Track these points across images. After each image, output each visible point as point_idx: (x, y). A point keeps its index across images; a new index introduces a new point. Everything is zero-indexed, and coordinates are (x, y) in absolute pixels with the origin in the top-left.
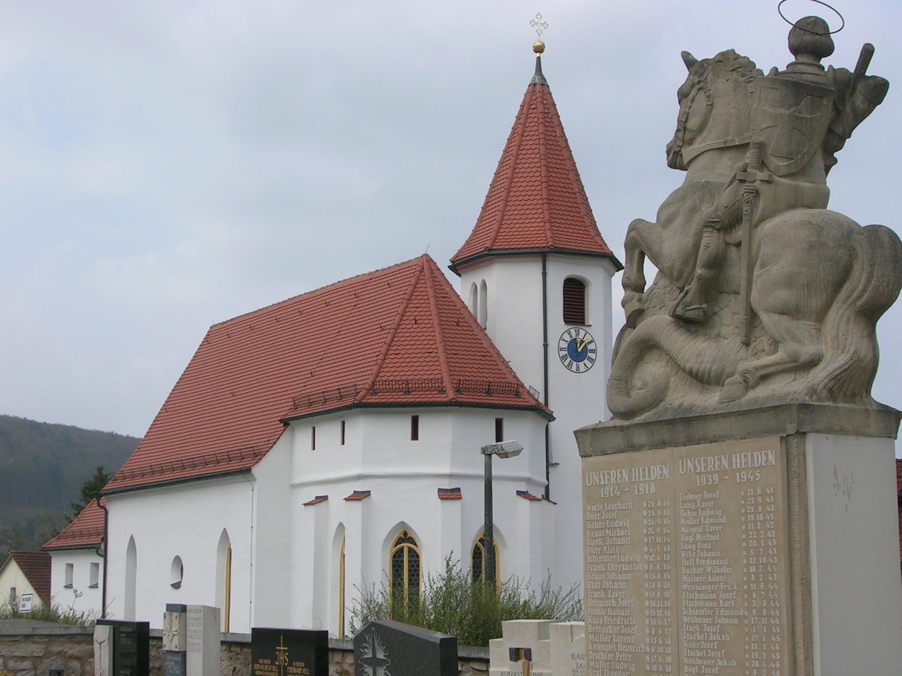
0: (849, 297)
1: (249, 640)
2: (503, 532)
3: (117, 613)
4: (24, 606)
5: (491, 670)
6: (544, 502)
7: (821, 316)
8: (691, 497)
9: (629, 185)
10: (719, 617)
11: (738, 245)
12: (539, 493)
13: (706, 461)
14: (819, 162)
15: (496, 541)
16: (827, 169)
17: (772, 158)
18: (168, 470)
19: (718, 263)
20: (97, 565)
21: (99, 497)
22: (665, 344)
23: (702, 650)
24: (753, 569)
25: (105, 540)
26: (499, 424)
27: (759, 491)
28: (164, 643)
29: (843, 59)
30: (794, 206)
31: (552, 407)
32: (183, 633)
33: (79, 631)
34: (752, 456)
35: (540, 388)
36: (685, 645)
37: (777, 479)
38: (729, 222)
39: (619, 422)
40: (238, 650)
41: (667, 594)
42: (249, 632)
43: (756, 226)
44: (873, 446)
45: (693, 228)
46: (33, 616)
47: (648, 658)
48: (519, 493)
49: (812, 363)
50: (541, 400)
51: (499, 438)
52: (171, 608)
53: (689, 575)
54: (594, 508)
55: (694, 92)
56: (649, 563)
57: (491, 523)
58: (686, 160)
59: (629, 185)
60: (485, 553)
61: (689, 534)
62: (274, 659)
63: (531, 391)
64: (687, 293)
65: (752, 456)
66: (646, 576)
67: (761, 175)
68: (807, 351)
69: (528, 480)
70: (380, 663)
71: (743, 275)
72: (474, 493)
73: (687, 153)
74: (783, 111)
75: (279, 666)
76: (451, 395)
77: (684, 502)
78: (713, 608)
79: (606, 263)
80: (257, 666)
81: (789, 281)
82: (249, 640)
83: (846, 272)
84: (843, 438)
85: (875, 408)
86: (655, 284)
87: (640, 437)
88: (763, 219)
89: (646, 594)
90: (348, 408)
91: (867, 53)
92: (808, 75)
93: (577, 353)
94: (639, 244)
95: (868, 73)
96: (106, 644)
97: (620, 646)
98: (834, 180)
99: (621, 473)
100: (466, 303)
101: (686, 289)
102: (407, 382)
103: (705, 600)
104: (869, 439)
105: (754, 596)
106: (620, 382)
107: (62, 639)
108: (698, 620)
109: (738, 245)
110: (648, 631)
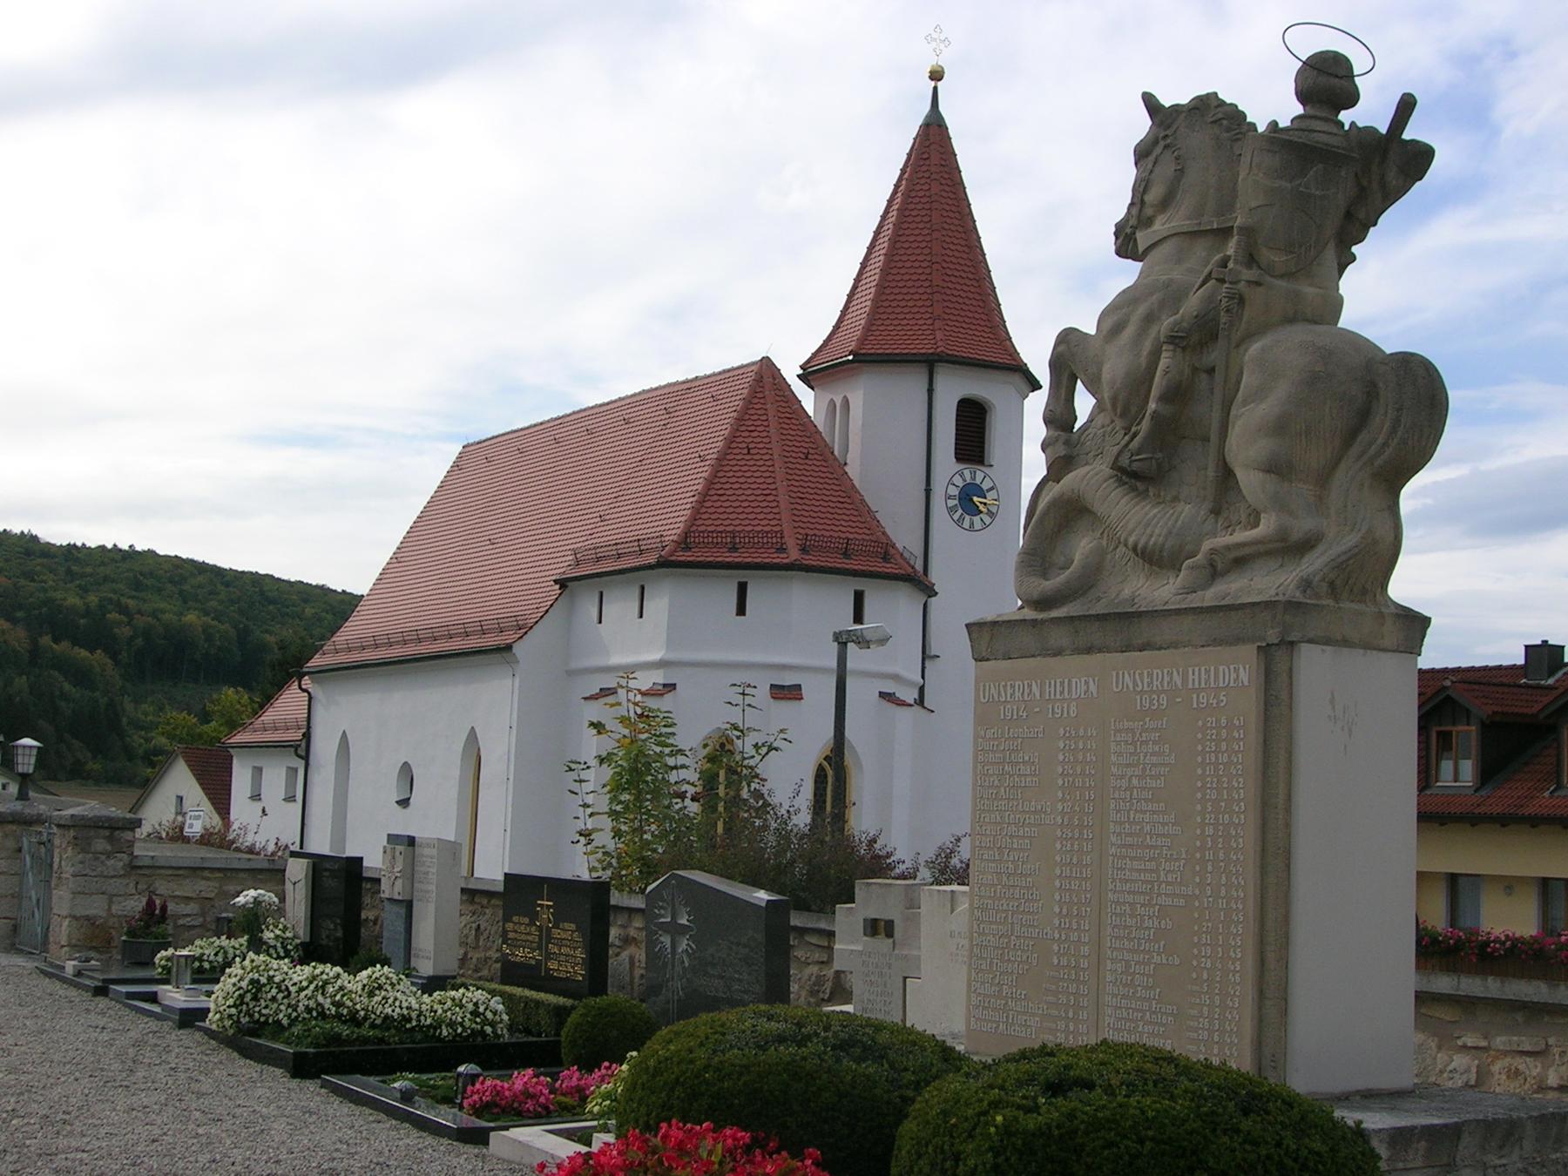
0: (1363, 453)
1: (501, 888)
2: (859, 750)
3: (320, 843)
4: (191, 826)
5: (837, 946)
6: (917, 708)
7: (1323, 479)
8: (1127, 724)
9: (1055, 268)
10: (1159, 895)
11: (1211, 371)
12: (910, 695)
13: (1150, 675)
14: (1330, 255)
15: (848, 759)
16: (1341, 270)
17: (1264, 251)
18: (398, 643)
19: (1177, 394)
20: (296, 770)
21: (301, 676)
22: (1100, 508)
23: (1133, 940)
24: (1209, 831)
25: (307, 736)
26: (859, 598)
27: (1223, 721)
28: (383, 887)
29: (1370, 111)
30: (1291, 320)
31: (936, 576)
32: (410, 874)
33: (266, 865)
34: (1216, 670)
35: (918, 550)
36: (1109, 930)
37: (1249, 706)
38: (1200, 336)
39: (1029, 614)
40: (485, 901)
41: (1087, 859)
42: (501, 878)
43: (1238, 346)
44: (1388, 664)
45: (1147, 346)
46: (206, 839)
47: (1056, 948)
48: (882, 694)
49: (1306, 545)
50: (919, 566)
51: (858, 618)
52: (393, 839)
53: (1119, 834)
54: (989, 734)
55: (1158, 150)
56: (1063, 813)
57: (843, 734)
58: (1141, 250)
59: (1055, 268)
60: (833, 776)
61: (1122, 777)
62: (534, 917)
63: (906, 555)
64: (1135, 435)
65: (1216, 670)
66: (1059, 833)
67: (1248, 274)
68: (1302, 525)
69: (896, 678)
70: (683, 930)
71: (1216, 415)
72: (820, 694)
73: (1143, 239)
74: (1284, 184)
75: (540, 928)
76: (794, 554)
77: (1117, 731)
78: (1152, 882)
79: (1017, 379)
80: (510, 926)
81: (1279, 427)
82: (501, 888)
83: (1363, 416)
84: (1345, 650)
85: (1393, 609)
86: (1090, 420)
87: (1059, 637)
88: (1250, 336)
89: (1058, 858)
90: (650, 567)
91: (1406, 106)
92: (1321, 136)
93: (968, 500)
94: (1070, 356)
95: (1407, 136)
96: (301, 885)
97: (1017, 928)
98: (1350, 284)
99: (1030, 686)
100: (821, 428)
101: (1134, 429)
102: (733, 534)
103: (1139, 871)
104: (1383, 655)
105: (1210, 868)
106: (1037, 557)
107: (241, 875)
108: (1130, 898)
109: (1211, 371)
110: (1057, 910)
